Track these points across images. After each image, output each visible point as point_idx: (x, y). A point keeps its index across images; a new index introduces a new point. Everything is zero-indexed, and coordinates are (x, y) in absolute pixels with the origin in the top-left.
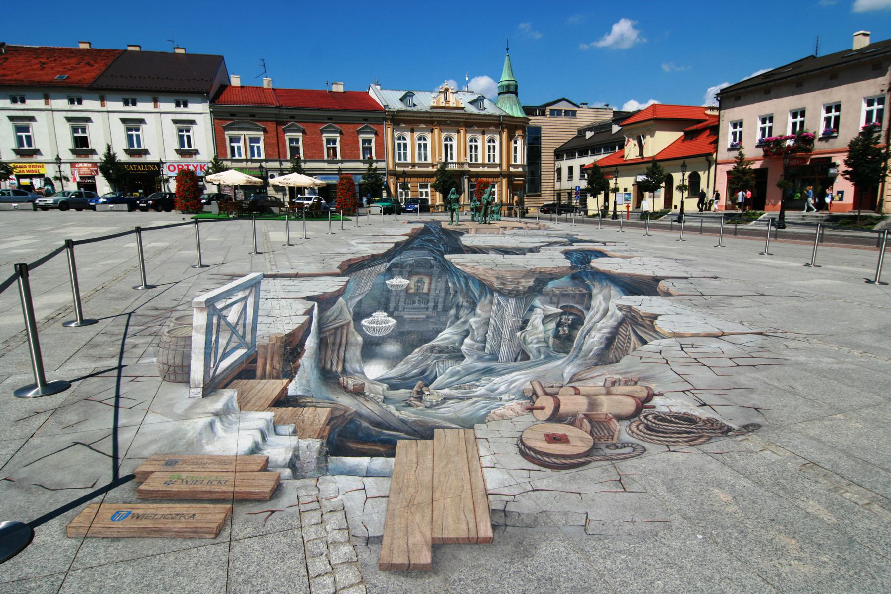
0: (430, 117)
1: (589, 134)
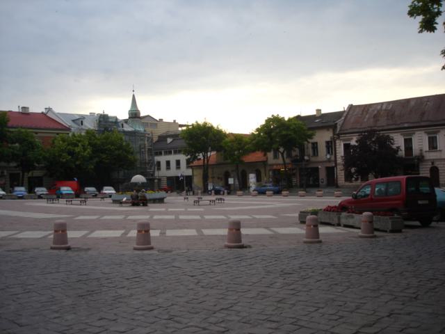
1: (169, 140)
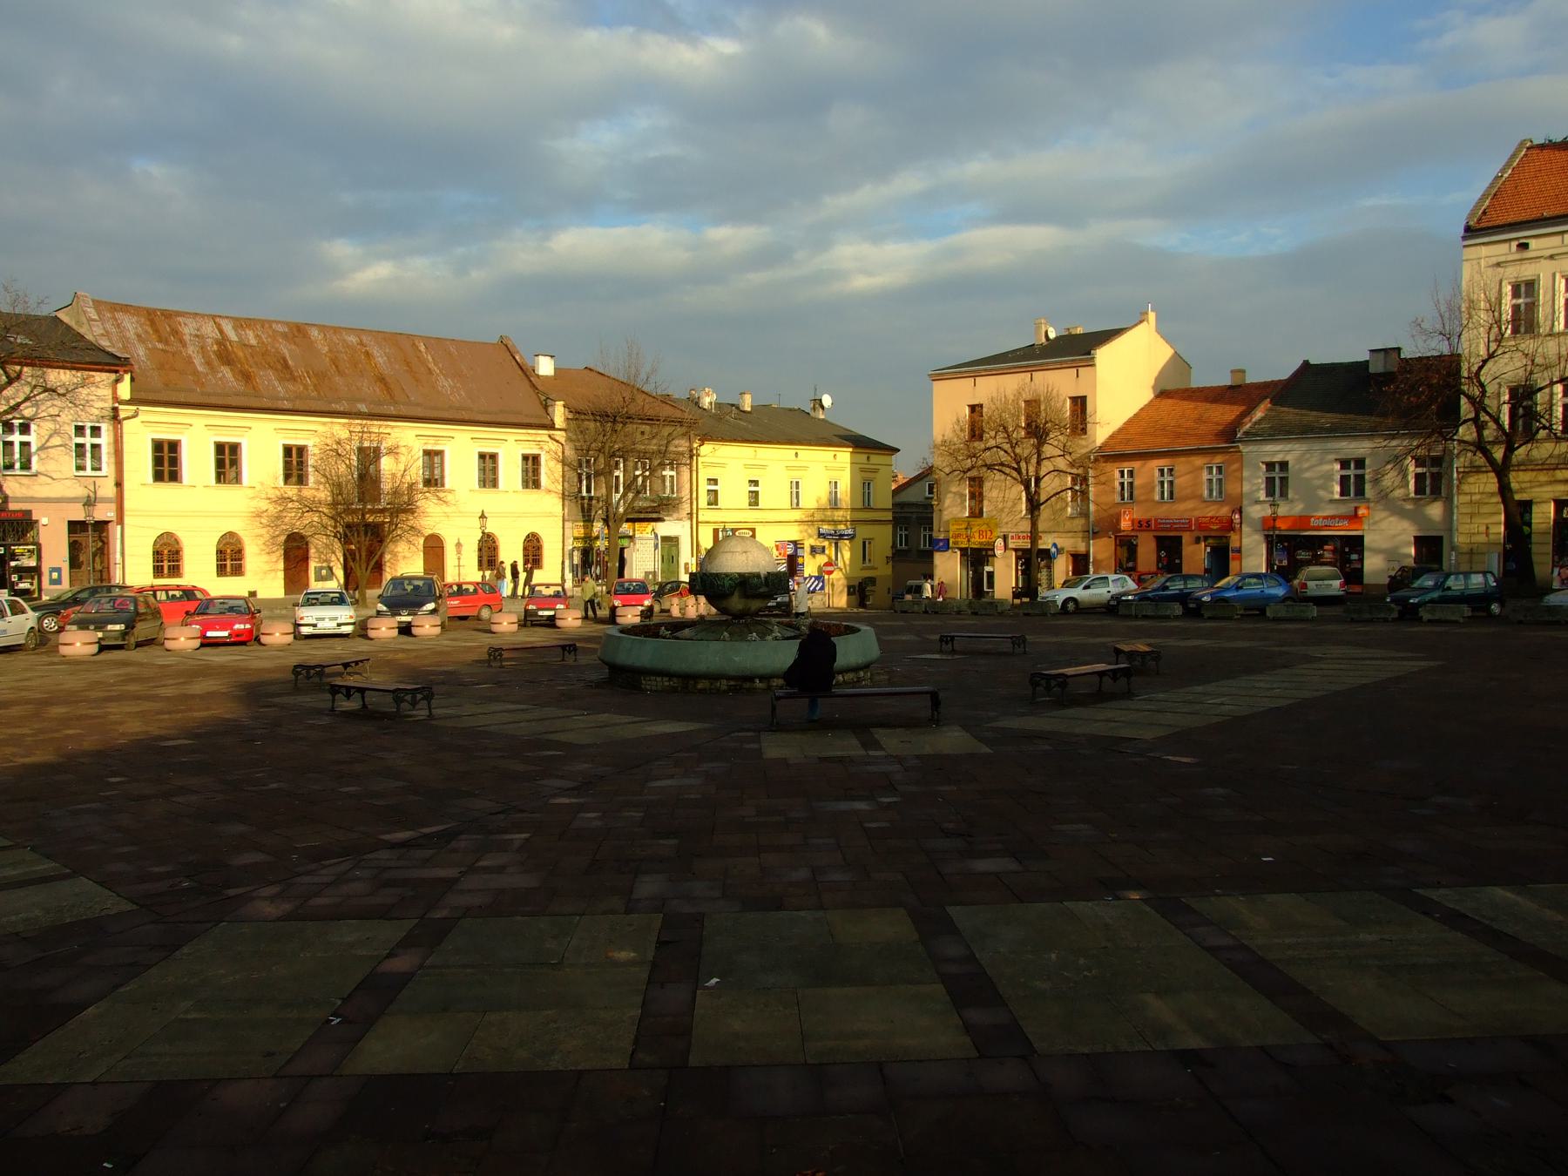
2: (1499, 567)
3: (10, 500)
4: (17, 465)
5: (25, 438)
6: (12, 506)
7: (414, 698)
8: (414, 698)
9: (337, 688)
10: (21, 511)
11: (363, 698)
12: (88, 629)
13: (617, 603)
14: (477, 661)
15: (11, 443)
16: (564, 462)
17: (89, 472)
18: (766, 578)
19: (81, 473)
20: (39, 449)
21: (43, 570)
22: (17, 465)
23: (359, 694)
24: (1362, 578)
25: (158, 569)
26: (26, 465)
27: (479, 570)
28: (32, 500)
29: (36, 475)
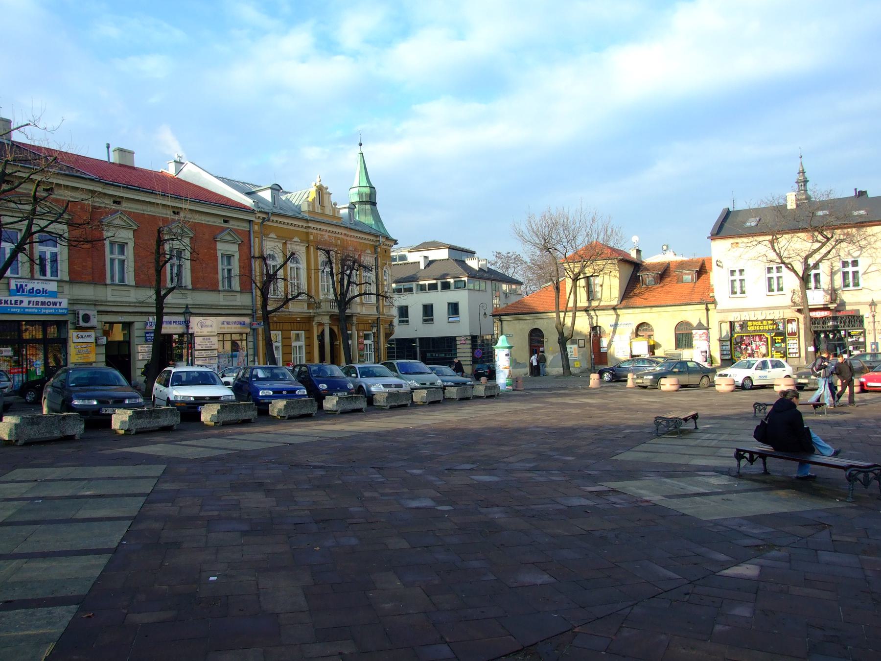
0: (306, 227)
2: (68, 466)
3: (846, 304)
4: (851, 284)
5: (855, 269)
6: (848, 308)
7: (866, 476)
8: (866, 476)
9: (742, 453)
10: (853, 310)
11: (765, 464)
12: (195, 397)
13: (863, 380)
14: (185, 430)
15: (848, 272)
16: (693, 259)
17: (851, 287)
18: (322, 369)
19: (772, 293)
20: (863, 274)
21: (867, 344)
22: (851, 284)
23: (761, 459)
24: (323, 407)
25: (362, 360)
26: (856, 284)
27: (878, 343)
28: (859, 303)
29: (862, 289)
